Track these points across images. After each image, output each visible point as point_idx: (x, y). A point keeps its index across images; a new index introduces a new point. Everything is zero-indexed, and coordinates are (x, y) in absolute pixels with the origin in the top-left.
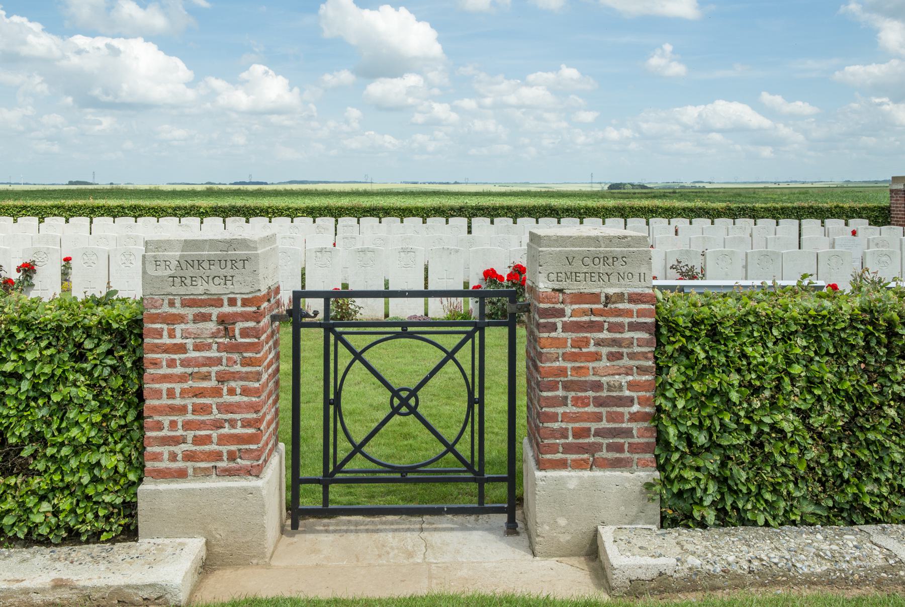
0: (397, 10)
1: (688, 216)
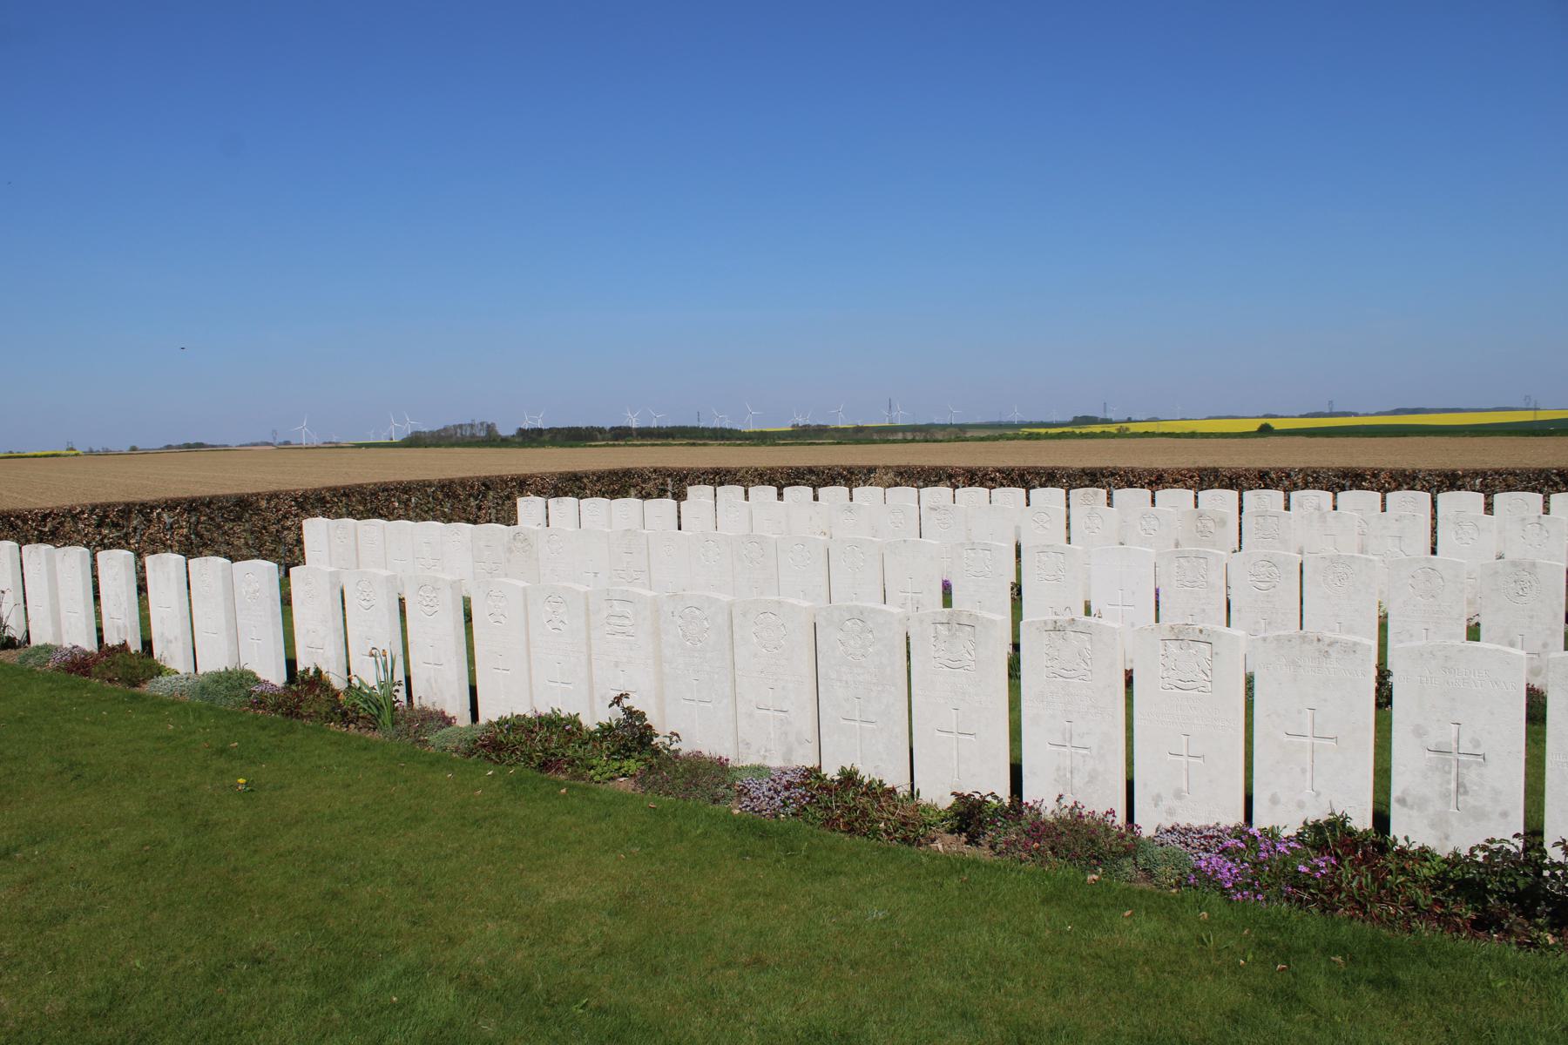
0: (843, 771)
1: (712, 483)
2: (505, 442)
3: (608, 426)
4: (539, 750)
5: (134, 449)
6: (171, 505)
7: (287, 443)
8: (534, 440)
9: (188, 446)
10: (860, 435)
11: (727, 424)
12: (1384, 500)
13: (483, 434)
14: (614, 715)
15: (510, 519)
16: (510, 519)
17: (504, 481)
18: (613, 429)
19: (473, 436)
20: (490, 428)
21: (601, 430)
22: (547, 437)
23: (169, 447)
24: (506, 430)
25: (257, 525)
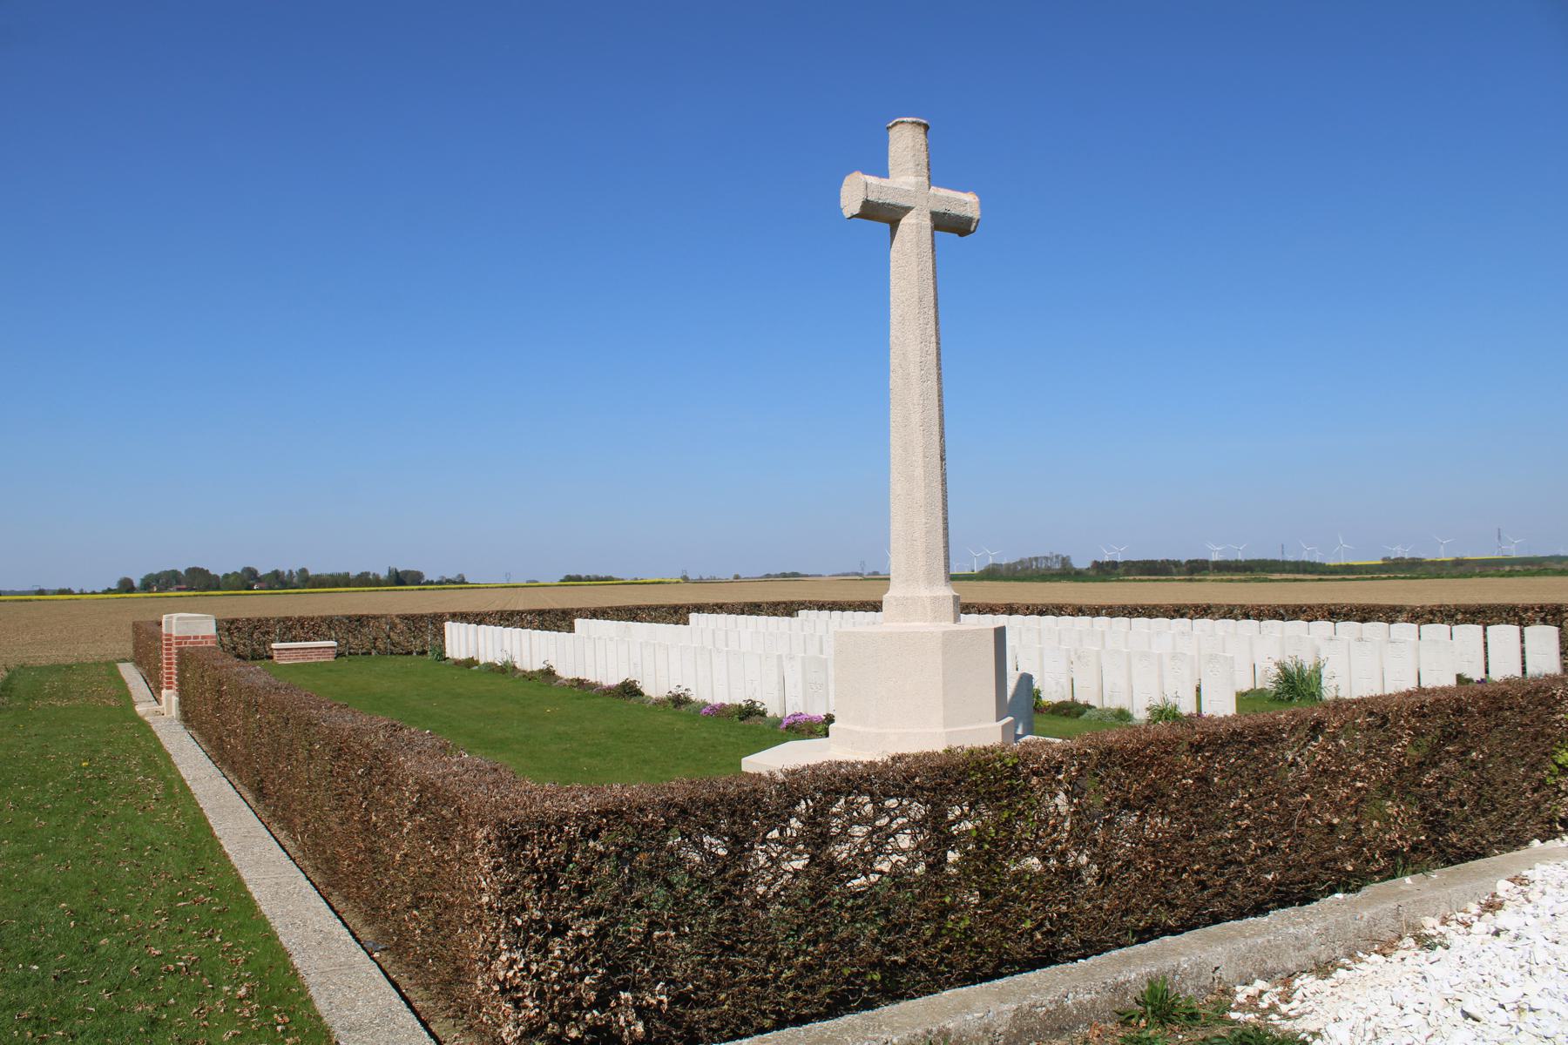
2: (376, 582)
3: (1184, 560)
4: (491, 668)
5: (737, 577)
6: (530, 612)
7: (876, 573)
8: (1108, 573)
9: (784, 575)
10: (1461, 568)
11: (1317, 558)
12: (1522, 632)
13: (1058, 566)
14: (543, 666)
15: (571, 629)
16: (571, 629)
17: (681, 607)
18: (1189, 562)
19: (1049, 568)
20: (1065, 561)
21: (1177, 564)
22: (1121, 570)
23: (768, 576)
24: (1081, 563)
25: (560, 620)
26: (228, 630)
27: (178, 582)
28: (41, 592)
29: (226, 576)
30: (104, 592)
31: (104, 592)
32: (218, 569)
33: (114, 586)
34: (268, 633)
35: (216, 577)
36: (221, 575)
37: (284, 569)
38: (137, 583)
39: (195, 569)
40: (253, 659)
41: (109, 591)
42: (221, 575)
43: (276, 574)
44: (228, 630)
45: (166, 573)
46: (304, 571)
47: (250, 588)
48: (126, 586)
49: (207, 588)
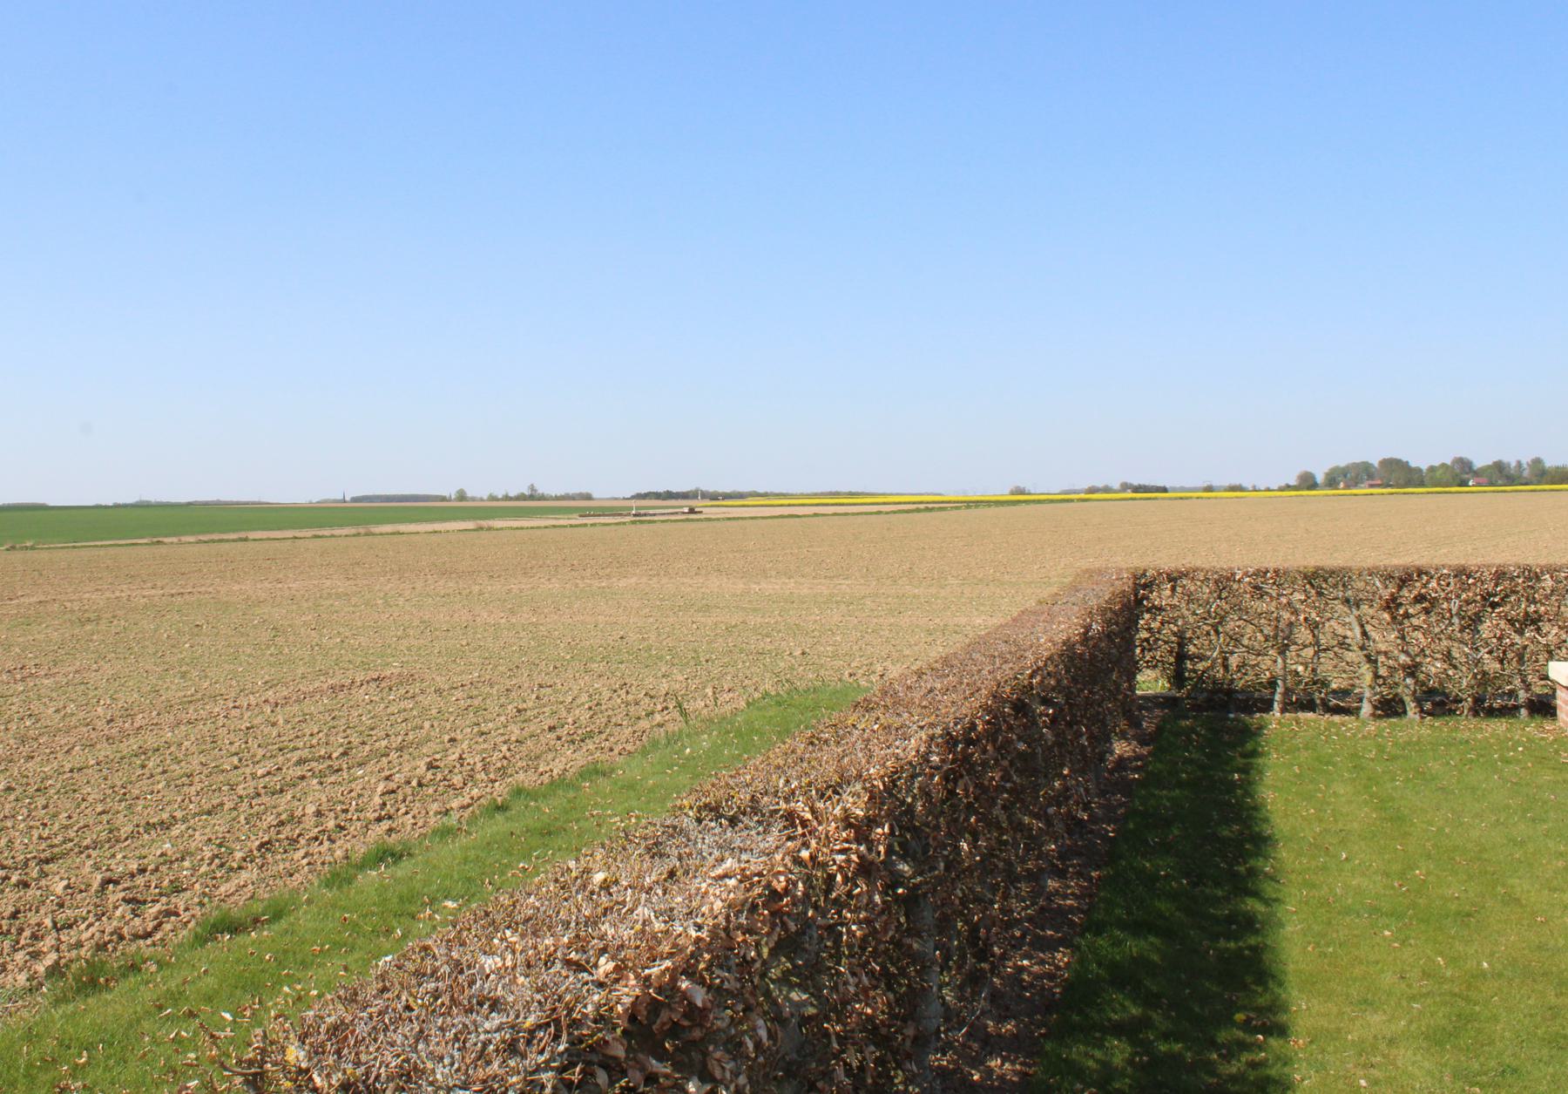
26: (1392, 604)
27: (1370, 476)
28: (1209, 489)
29: (1432, 469)
30: (1281, 489)
31: (1281, 489)
32: (1421, 460)
33: (1293, 482)
34: (1533, 621)
35: (1419, 470)
36: (1424, 467)
37: (1510, 459)
38: (1320, 478)
39: (1398, 462)
40: (1482, 709)
41: (1288, 487)
42: (1424, 467)
43: (1499, 467)
44: (1392, 604)
45: (1356, 466)
46: (1537, 462)
47: (1464, 483)
48: (1308, 482)
49: (1408, 484)
